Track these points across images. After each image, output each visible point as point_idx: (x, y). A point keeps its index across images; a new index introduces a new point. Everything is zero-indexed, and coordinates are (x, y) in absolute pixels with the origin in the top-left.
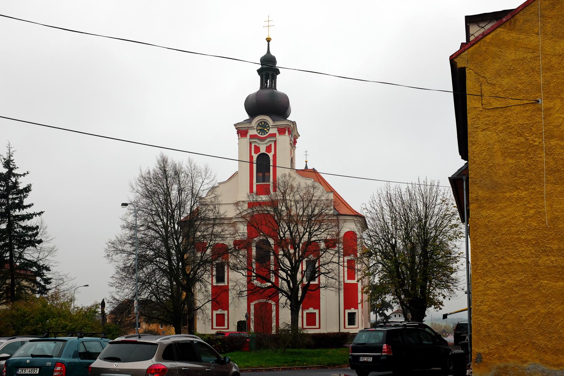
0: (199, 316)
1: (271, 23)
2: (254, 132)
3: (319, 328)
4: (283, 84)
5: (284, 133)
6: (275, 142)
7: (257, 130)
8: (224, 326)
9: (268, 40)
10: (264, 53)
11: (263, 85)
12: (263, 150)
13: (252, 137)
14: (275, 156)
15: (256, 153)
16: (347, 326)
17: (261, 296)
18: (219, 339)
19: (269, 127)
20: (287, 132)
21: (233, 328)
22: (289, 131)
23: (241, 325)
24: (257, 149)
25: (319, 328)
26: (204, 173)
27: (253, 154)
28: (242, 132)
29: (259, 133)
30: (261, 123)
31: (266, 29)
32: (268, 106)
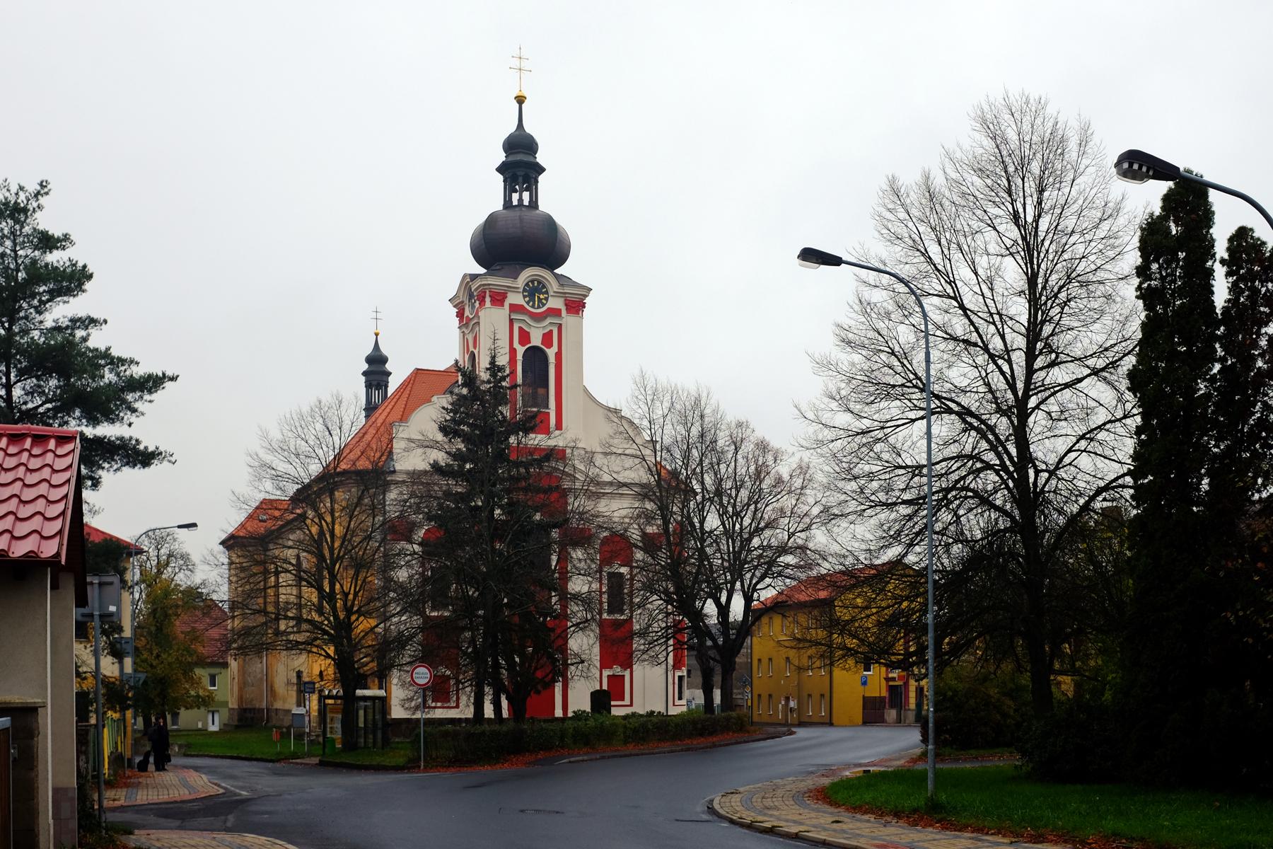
1: (525, 64)
2: (516, 299)
3: (631, 705)
9: (520, 100)
10: (512, 128)
12: (536, 341)
13: (514, 308)
14: (559, 356)
15: (522, 343)
19: (547, 292)
24: (524, 337)
25: (631, 705)
27: (516, 345)
30: (532, 281)
32: (519, 248)
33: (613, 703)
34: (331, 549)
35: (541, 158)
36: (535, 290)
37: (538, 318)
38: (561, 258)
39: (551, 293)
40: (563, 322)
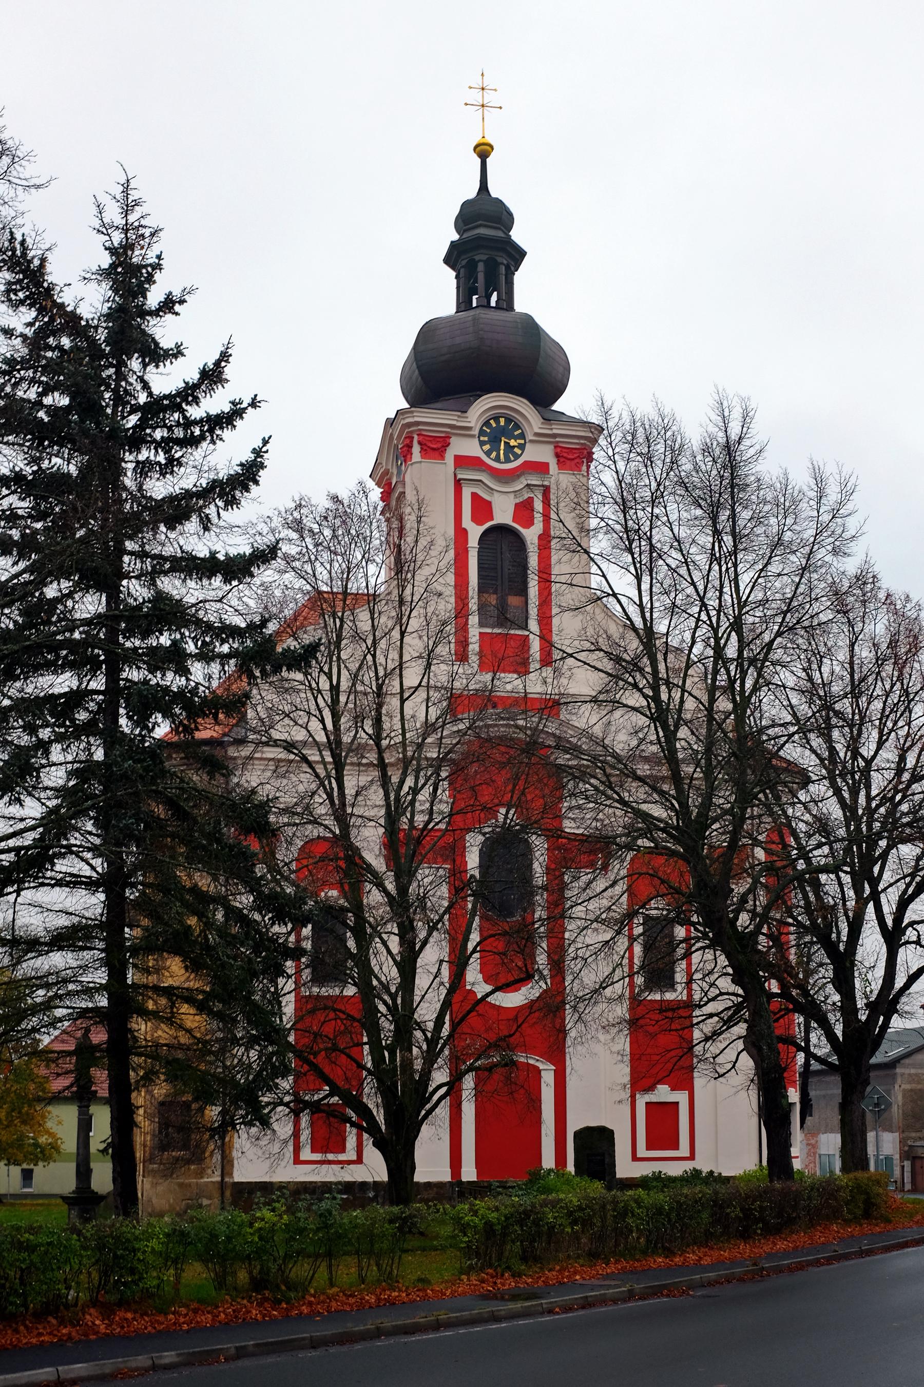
1: (489, 97)
2: (471, 448)
6: (546, 491)
7: (482, 443)
8: (676, 1147)
9: (483, 152)
10: (472, 192)
12: (503, 514)
13: (462, 461)
16: (306, 1154)
24: (482, 509)
25: (692, 1157)
29: (488, 453)
30: (496, 419)
33: (104, 596)
35: (516, 235)
36: (499, 431)
38: (558, 390)
39: (530, 436)
40: (551, 481)
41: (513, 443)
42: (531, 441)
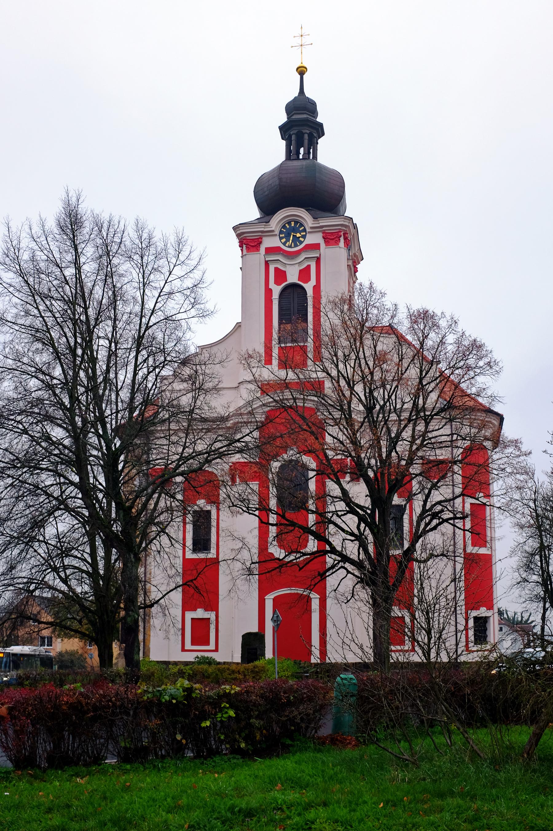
0: (156, 620)
3: (216, 650)
4: (329, 153)
5: (337, 242)
6: (318, 260)
7: (281, 238)
8: (208, 644)
9: (302, 71)
10: (296, 93)
11: (291, 154)
12: (293, 277)
13: (269, 251)
14: (317, 289)
15: (278, 282)
17: (290, 579)
18: (226, 696)
19: (305, 230)
20: (342, 239)
21: (230, 652)
22: (346, 239)
23: (252, 644)
24: (281, 275)
25: (216, 650)
26: (171, 251)
27: (272, 285)
28: (248, 241)
29: (284, 244)
30: (289, 223)
31: (298, 50)
32: (301, 194)
34: (101, 508)
37: (291, 255)
39: (308, 230)
41: (298, 235)
42: (309, 232)
